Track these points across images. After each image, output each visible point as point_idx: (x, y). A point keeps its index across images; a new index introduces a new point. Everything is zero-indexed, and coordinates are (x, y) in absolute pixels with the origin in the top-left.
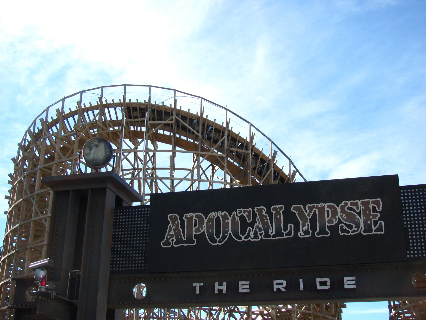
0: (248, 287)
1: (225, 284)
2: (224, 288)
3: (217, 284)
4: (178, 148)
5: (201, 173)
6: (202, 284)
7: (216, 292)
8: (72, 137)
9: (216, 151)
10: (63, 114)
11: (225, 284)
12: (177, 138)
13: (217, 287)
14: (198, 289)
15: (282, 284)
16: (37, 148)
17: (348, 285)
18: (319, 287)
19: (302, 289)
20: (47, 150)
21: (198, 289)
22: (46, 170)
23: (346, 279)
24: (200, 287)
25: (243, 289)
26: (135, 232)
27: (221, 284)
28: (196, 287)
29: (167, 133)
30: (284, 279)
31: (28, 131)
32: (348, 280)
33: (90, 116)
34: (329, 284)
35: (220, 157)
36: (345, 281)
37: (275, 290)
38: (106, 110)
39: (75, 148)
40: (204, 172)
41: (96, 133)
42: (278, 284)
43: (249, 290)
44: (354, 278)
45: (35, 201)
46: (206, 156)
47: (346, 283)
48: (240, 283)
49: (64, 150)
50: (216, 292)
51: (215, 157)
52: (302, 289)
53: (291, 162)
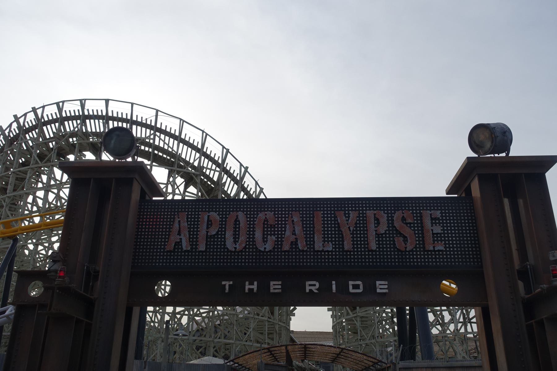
0: (280, 287)
1: (256, 283)
2: (255, 287)
3: (247, 283)
4: (154, 164)
5: (175, 188)
6: (231, 283)
7: (247, 291)
8: (50, 144)
9: (190, 169)
10: (25, 128)
11: (256, 283)
12: (155, 154)
13: (247, 287)
14: (227, 287)
15: (315, 285)
16: (20, 148)
17: (381, 289)
18: (351, 290)
19: (335, 292)
20: (22, 153)
21: (227, 287)
22: (20, 173)
23: (378, 283)
24: (229, 285)
25: (274, 289)
26: (161, 227)
27: (251, 283)
28: (225, 285)
29: (143, 147)
30: (317, 281)
31: (34, 110)
32: (380, 285)
33: (70, 126)
34: (361, 287)
35: (194, 174)
36: (377, 285)
37: (307, 291)
38: (88, 121)
39: (53, 155)
40: (178, 187)
41: (76, 142)
42: (310, 285)
43: (280, 291)
44: (387, 283)
45: (5, 204)
46: (181, 173)
47: (378, 287)
48: (272, 283)
49: (41, 157)
50: (247, 291)
51: (189, 173)
52: (335, 292)
53: (257, 183)
